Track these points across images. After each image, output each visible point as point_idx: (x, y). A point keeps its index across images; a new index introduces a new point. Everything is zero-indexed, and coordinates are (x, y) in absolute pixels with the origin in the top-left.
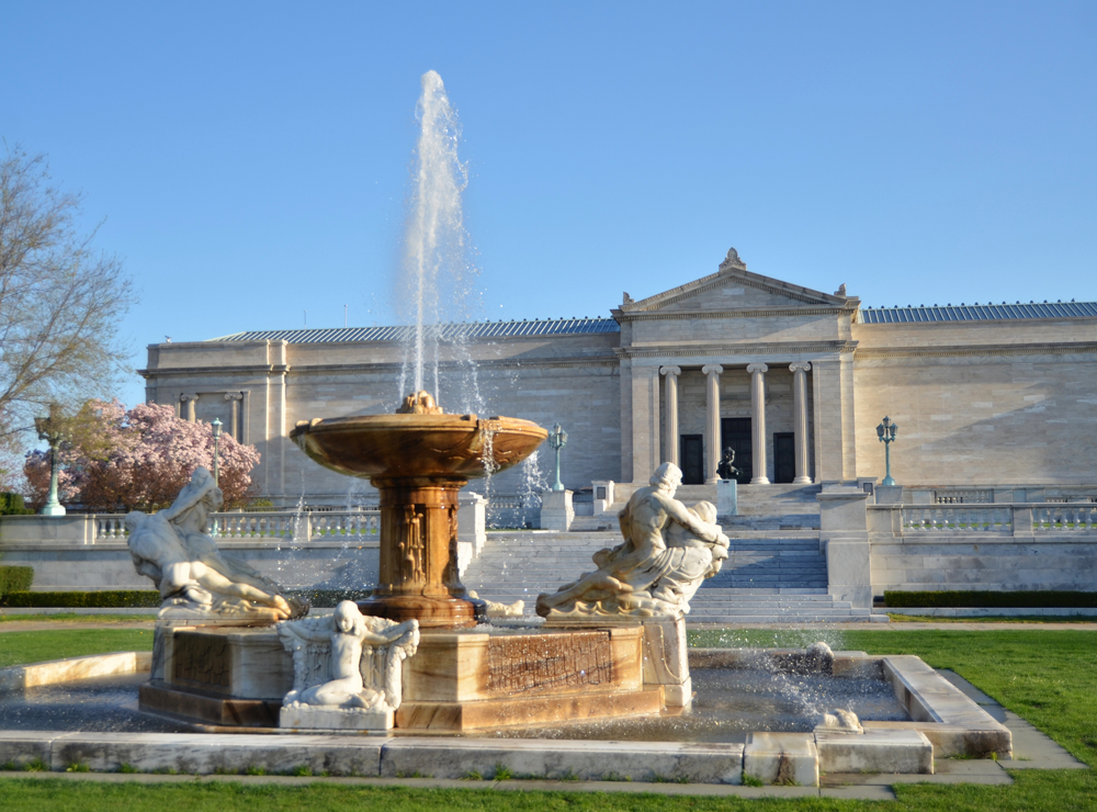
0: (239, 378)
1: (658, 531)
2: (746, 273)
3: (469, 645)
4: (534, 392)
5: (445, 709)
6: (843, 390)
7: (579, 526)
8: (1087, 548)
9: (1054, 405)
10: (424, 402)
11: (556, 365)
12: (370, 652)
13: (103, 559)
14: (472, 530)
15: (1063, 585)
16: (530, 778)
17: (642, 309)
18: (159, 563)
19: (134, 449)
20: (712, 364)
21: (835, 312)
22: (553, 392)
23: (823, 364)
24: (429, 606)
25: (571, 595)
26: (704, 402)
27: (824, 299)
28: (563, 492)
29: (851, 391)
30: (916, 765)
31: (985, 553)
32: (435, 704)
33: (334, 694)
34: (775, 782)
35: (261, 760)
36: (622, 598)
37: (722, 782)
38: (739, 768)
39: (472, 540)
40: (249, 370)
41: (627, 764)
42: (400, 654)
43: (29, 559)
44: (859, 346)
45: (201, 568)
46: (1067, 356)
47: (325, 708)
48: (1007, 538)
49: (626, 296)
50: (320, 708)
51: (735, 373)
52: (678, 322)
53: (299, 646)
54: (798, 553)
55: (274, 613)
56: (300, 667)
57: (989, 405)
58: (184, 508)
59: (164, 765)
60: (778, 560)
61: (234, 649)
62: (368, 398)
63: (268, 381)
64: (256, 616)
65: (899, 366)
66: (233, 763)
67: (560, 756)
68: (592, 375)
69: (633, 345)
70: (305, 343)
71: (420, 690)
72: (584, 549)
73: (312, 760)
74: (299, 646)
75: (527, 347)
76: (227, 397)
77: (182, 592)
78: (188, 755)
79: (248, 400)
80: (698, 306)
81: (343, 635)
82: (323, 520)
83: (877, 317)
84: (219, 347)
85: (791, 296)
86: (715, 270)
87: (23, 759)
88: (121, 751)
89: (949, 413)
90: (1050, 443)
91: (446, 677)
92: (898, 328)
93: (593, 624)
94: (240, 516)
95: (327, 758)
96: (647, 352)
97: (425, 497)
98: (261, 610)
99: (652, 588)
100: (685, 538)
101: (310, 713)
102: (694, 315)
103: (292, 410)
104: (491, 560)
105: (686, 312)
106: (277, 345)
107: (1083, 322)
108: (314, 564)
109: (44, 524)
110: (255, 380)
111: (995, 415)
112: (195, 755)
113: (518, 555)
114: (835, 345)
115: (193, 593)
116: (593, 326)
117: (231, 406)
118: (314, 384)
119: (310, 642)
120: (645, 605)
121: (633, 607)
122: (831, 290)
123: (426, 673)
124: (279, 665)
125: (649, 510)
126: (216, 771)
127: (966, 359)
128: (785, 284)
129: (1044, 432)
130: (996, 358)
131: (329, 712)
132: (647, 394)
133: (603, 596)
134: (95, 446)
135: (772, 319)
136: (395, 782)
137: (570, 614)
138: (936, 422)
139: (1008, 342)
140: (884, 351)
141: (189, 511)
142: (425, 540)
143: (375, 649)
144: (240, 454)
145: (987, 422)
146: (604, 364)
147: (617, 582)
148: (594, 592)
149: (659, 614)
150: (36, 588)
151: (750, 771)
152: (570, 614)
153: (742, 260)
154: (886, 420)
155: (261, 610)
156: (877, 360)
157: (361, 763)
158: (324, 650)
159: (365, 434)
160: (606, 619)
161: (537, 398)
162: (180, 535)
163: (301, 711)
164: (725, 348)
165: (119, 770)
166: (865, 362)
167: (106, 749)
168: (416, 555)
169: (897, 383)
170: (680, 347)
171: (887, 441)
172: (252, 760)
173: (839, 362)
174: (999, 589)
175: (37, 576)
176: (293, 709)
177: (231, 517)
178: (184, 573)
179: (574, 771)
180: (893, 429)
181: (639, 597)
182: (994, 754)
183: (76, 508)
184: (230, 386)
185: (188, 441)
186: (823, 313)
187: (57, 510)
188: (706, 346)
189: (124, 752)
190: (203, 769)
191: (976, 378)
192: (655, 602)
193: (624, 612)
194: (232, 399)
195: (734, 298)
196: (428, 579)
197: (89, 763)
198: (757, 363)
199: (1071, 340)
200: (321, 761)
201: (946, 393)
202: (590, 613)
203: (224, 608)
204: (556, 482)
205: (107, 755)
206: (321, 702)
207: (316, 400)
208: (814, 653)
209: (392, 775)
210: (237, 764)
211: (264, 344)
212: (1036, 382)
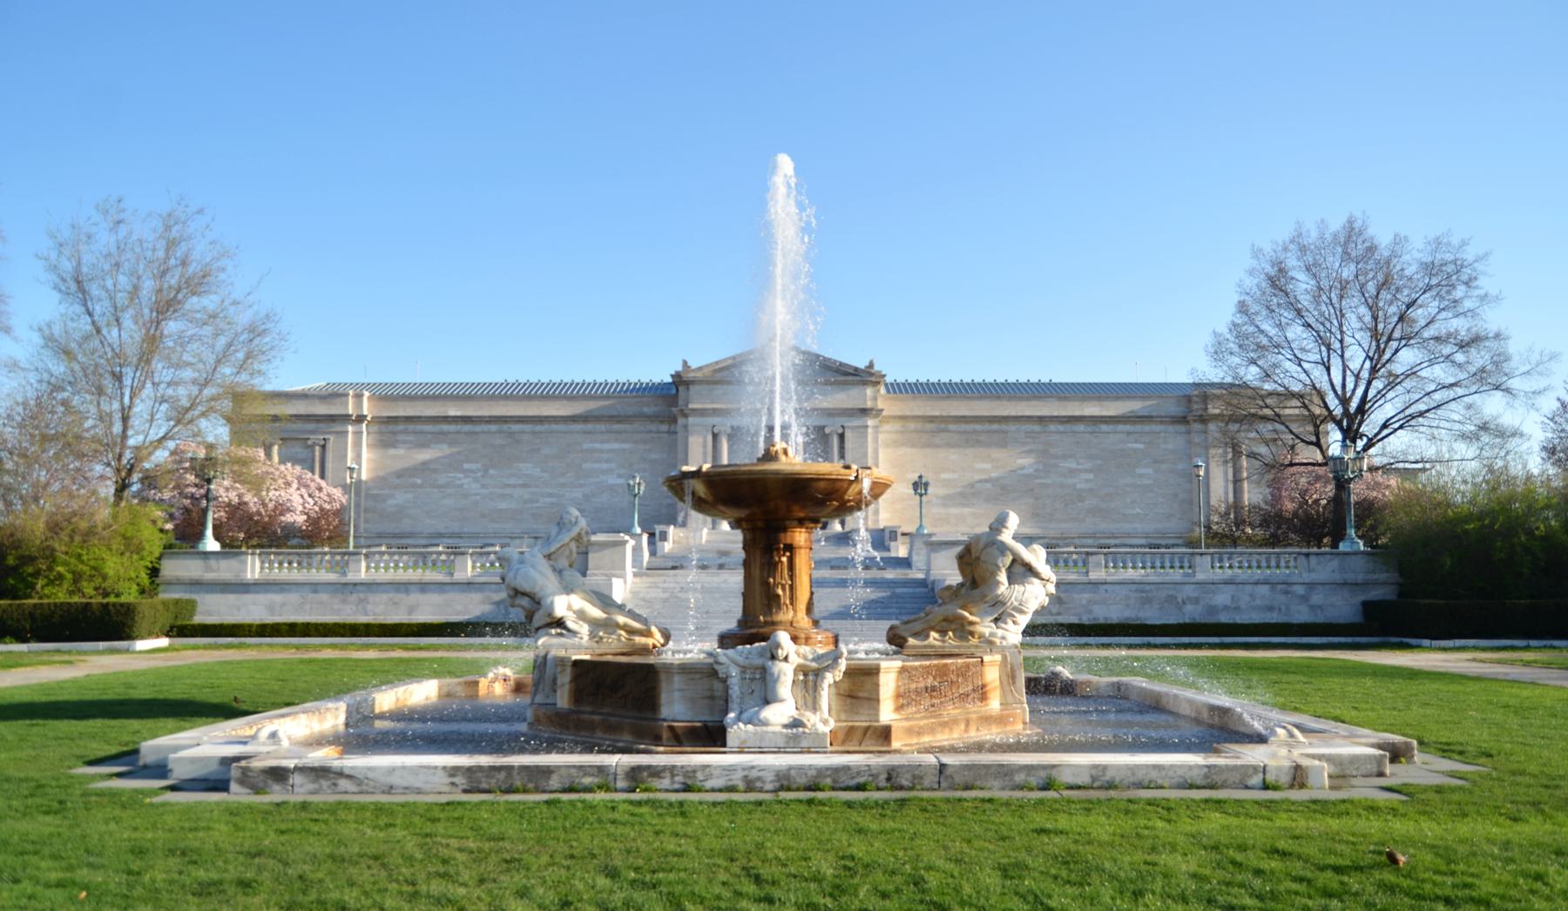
0: (322, 425)
1: (1004, 570)
3: (888, 671)
4: (598, 446)
6: (870, 450)
7: (654, 565)
8: (1148, 588)
10: (785, 452)
11: (619, 422)
12: (801, 678)
13: (266, 592)
14: (623, 568)
16: (1079, 787)
17: (699, 375)
18: (538, 596)
19: (227, 490)
21: (865, 383)
22: (616, 446)
23: (853, 428)
24: (803, 636)
25: (925, 626)
27: (856, 372)
28: (640, 535)
29: (876, 451)
30: (1375, 770)
31: (1066, 591)
32: (867, 724)
33: (778, 714)
34: (1291, 786)
35: (826, 777)
36: (971, 628)
37: (1247, 787)
38: (1261, 775)
39: (623, 576)
40: (332, 419)
41: (1164, 773)
42: (829, 678)
43: (191, 592)
44: (884, 413)
45: (577, 601)
46: (1052, 427)
47: (770, 729)
48: (1084, 579)
49: (685, 363)
50: (764, 728)
53: (734, 672)
54: (911, 590)
55: (650, 641)
56: (735, 691)
57: (987, 466)
58: (558, 545)
59: (730, 783)
60: (894, 596)
61: (663, 676)
62: (445, 446)
63: (350, 428)
64: (634, 645)
65: (916, 431)
66: (798, 780)
67: (1105, 768)
68: (651, 432)
69: (690, 406)
70: (385, 395)
71: (845, 711)
72: (723, 585)
73: (875, 776)
74: (734, 672)
75: (592, 405)
76: (310, 442)
77: (560, 623)
78: (754, 774)
79: (330, 446)
81: (777, 662)
82: (405, 558)
83: (899, 389)
84: (303, 396)
87: (587, 781)
89: (954, 472)
90: (1037, 499)
91: (869, 699)
92: (915, 398)
93: (947, 651)
94: (325, 554)
95: (889, 774)
96: (702, 413)
97: (792, 538)
98: (638, 640)
99: (996, 620)
100: (1025, 577)
101: (755, 734)
103: (372, 456)
106: (359, 396)
107: (1066, 399)
108: (476, 597)
109: (207, 558)
110: (338, 428)
111: (994, 475)
112: (761, 774)
113: (664, 590)
114: (864, 412)
115: (570, 624)
116: (657, 389)
117: (313, 452)
118: (394, 433)
119: (744, 669)
120: (992, 634)
121: (981, 636)
122: (862, 365)
124: (711, 690)
125: (996, 552)
126: (782, 788)
127: (970, 427)
129: (1032, 490)
130: (995, 427)
131: (774, 733)
132: (701, 450)
133: (953, 627)
134: (188, 485)
136: (959, 794)
137: (926, 643)
138: (945, 480)
139: (1005, 413)
140: (903, 418)
142: (792, 577)
143: (805, 675)
144: (329, 495)
145: (986, 481)
146: (662, 422)
147: (966, 614)
148: (944, 624)
149: (1004, 643)
150: (198, 619)
151: (1270, 778)
152: (926, 643)
154: (920, 477)
155: (638, 640)
156: (897, 426)
157: (921, 778)
158: (758, 676)
159: (759, 480)
160: (958, 647)
161: (601, 451)
162: (554, 570)
163: (746, 732)
165: (687, 789)
166: (887, 427)
167: (672, 769)
168: (784, 589)
169: (913, 446)
171: (921, 495)
172: (816, 777)
173: (867, 427)
174: (1077, 621)
175: (199, 608)
176: (737, 731)
177: (317, 554)
178: (563, 605)
179: (1117, 780)
180: (926, 485)
181: (985, 627)
182: (1403, 760)
183: (230, 546)
184: (313, 432)
185: (281, 481)
186: (854, 384)
187: (211, 544)
189: (691, 772)
190: (769, 787)
191: (978, 443)
192: (1000, 632)
193: (974, 641)
194: (315, 444)
196: (795, 611)
197: (656, 783)
199: (1056, 414)
200: (884, 776)
201: (953, 456)
202: (944, 641)
203: (601, 638)
204: (633, 525)
205: (673, 776)
206: (765, 723)
207: (395, 447)
209: (953, 788)
210: (802, 781)
211: (347, 395)
212: (1027, 448)
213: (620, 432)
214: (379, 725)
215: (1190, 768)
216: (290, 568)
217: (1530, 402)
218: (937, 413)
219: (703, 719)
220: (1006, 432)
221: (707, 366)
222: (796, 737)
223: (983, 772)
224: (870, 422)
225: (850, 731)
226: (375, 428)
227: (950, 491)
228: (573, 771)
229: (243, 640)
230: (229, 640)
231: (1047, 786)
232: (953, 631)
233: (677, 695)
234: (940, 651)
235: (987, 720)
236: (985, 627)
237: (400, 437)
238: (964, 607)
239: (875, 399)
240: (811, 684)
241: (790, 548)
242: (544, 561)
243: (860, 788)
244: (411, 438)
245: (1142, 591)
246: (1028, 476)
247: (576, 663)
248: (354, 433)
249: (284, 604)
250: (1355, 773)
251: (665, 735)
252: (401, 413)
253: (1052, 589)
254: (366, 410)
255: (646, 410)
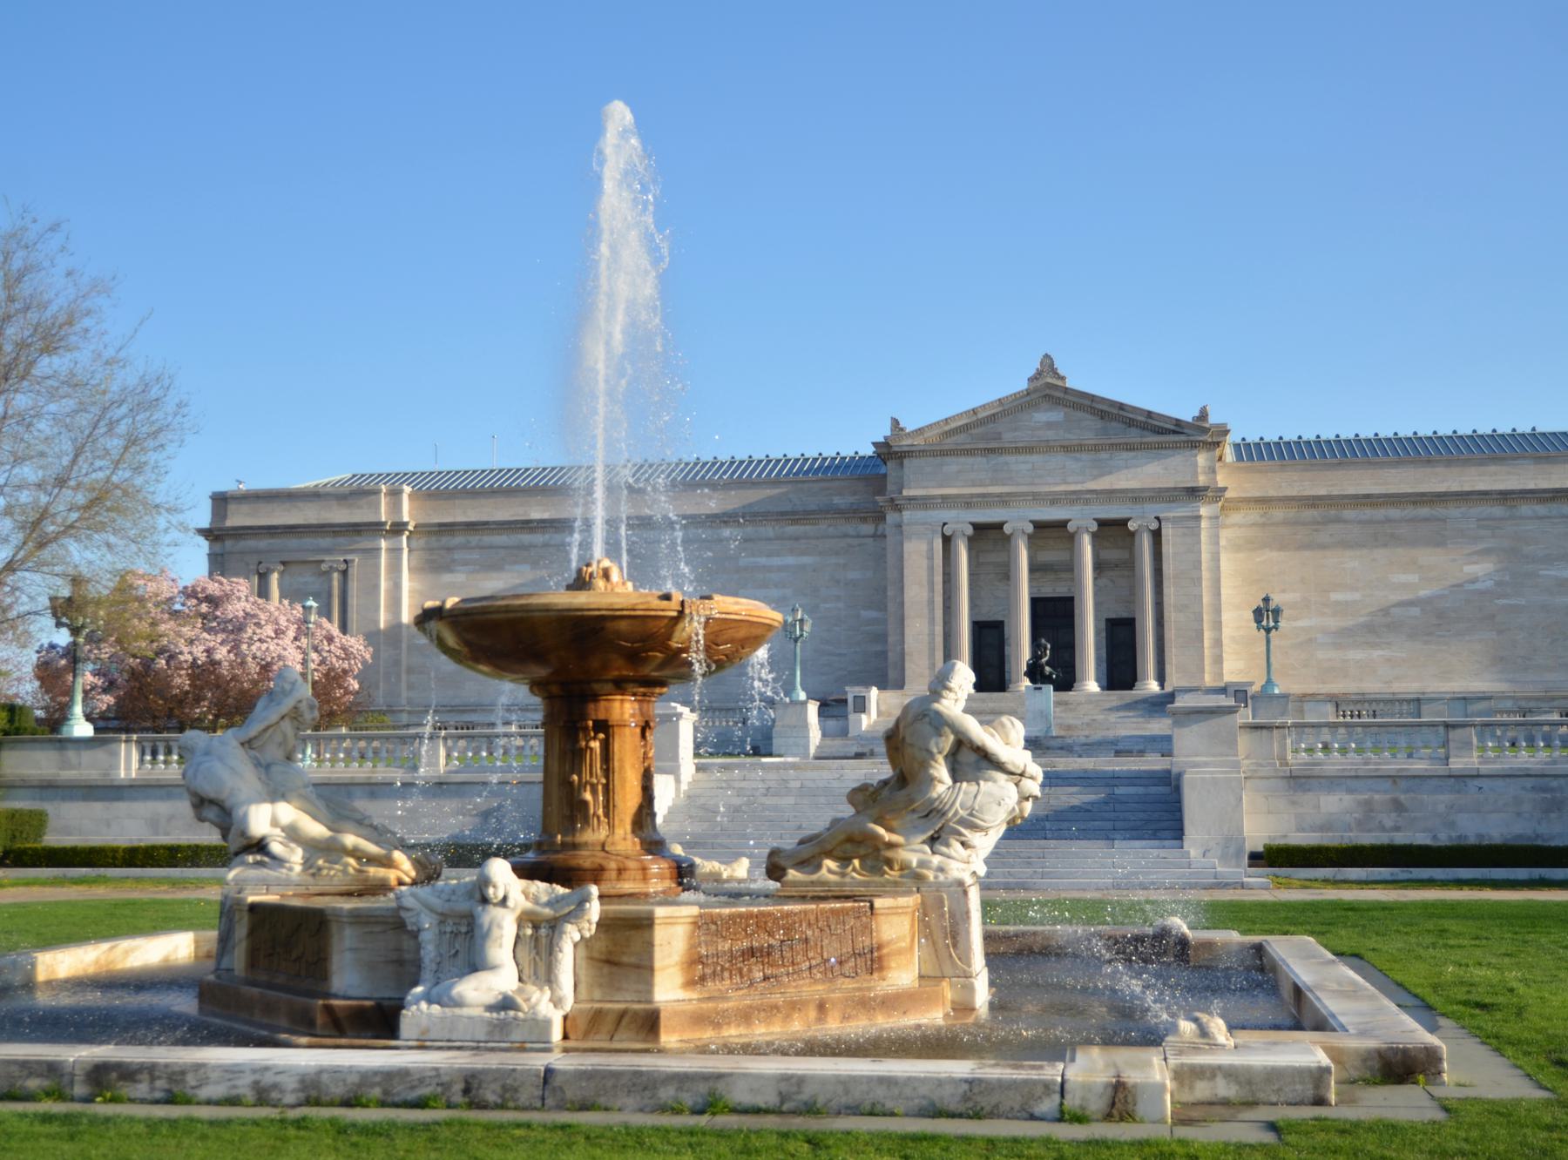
0: (341, 540)
1: (940, 759)
2: (1066, 390)
3: (671, 922)
4: (763, 561)
5: (636, 1013)
7: (827, 752)
8: (1554, 784)
9: (1507, 578)
10: (606, 574)
11: (795, 522)
12: (529, 932)
13: (147, 798)
14: (675, 757)
15: (1520, 836)
16: (758, 1111)
17: (918, 441)
18: (227, 804)
19: (191, 642)
20: (1018, 520)
21: (1194, 446)
22: (790, 560)
23: (1176, 521)
24: (613, 865)
26: (1006, 574)
27: (1178, 427)
28: (804, 703)
29: (1216, 559)
30: (1310, 1093)
32: (622, 1006)
33: (476, 991)
34: (1108, 1117)
35: (373, 1085)
36: (889, 854)
37: (1032, 1117)
38: (1057, 1097)
39: (674, 771)
40: (356, 529)
41: (896, 1091)
42: (571, 935)
43: (42, 799)
44: (1228, 494)
45: (287, 812)
46: (1525, 509)
47: (465, 1011)
48: (1440, 769)
49: (895, 422)
50: (457, 1011)
51: (1050, 532)
52: (970, 460)
53: (427, 923)
54: (1141, 790)
55: (391, 875)
56: (429, 952)
57: (1413, 578)
58: (260, 727)
59: (234, 1092)
60: (1111, 800)
61: (334, 928)
62: (526, 568)
63: (383, 544)
64: (366, 880)
65: (1286, 523)
67: (800, 1081)
68: (846, 536)
69: (905, 493)
70: (434, 490)
71: (601, 985)
73: (446, 1086)
74: (427, 923)
76: (324, 567)
77: (260, 846)
78: (268, 1079)
79: (354, 571)
80: (998, 437)
81: (491, 908)
83: (1255, 453)
84: (313, 495)
85: (1131, 423)
86: (1023, 385)
87: (33, 1084)
88: (174, 1073)
91: (638, 967)
93: (847, 890)
94: (342, 738)
95: (467, 1082)
96: (925, 503)
97: (607, 710)
98: (374, 872)
99: (933, 841)
100: (979, 769)
101: (443, 1019)
102: (992, 451)
103: (417, 585)
104: (702, 801)
105: (981, 446)
106: (395, 494)
107: (1548, 460)
109: (62, 748)
110: (365, 543)
111: (1422, 593)
112: (279, 1079)
113: (740, 792)
115: (276, 848)
117: (330, 580)
118: (449, 549)
119: (443, 917)
120: (922, 864)
121: (904, 867)
122: (1187, 414)
123: (609, 962)
124: (399, 950)
125: (928, 729)
126: (309, 1102)
127: (1380, 513)
128: (1121, 406)
130: (1424, 511)
131: (470, 1018)
132: (925, 563)
133: (862, 851)
134: (136, 638)
135: (1104, 455)
137: (814, 877)
138: (1338, 603)
140: (1263, 501)
141: (270, 731)
142: (607, 772)
143: (536, 927)
144: (344, 649)
145: (1411, 603)
146: (864, 520)
147: (881, 831)
148: (848, 846)
149: (942, 877)
150: (52, 839)
151: (1072, 1102)
152: (814, 877)
153: (1061, 372)
154: (1266, 600)
155: (374, 872)
156: (1254, 515)
157: (516, 1090)
158: (464, 929)
161: (769, 569)
162: (257, 764)
163: (430, 1016)
164: (1036, 498)
165: (171, 1099)
166: (1236, 517)
167: (151, 1070)
168: (594, 792)
169: (1282, 547)
170: (972, 496)
171: (1268, 630)
172: (360, 1085)
173: (1199, 518)
175: (52, 823)
176: (419, 1013)
177: (331, 738)
178: (262, 819)
180: (1277, 612)
181: (913, 852)
182: (1421, 1078)
183: (109, 725)
184: (328, 551)
186: (1176, 447)
188: (1008, 494)
189: (176, 1075)
190: (290, 1099)
191: (1394, 540)
195: (1050, 425)
196: (611, 826)
198: (1082, 519)
199: (1531, 486)
201: (1351, 562)
202: (843, 875)
203: (320, 869)
204: (794, 688)
205: (153, 1079)
206: (458, 1003)
208: (1163, 934)
209: (561, 1107)
210: (338, 1091)
211: (377, 492)
213: (797, 539)
214: (43, 999)
215: (940, 1083)
216: (334, 761)
217: (630, 465)
218: (1323, 492)
219: (377, 995)
220: (1444, 520)
221: (931, 426)
222: (502, 1026)
223: (610, 1084)
224: (1204, 511)
225: (596, 1018)
226: (420, 542)
227: (1349, 622)
228: (14, 1070)
229: (102, 871)
230: (84, 870)
231: (710, 1105)
232: (862, 859)
233: (348, 956)
234: (836, 891)
235: (891, 1002)
236: (913, 852)
237: (457, 555)
238: (879, 821)
239: (1213, 471)
240: (544, 941)
241: (604, 727)
242: (240, 752)
243: (421, 1104)
244: (475, 556)
245: (1544, 790)
246: (1482, 593)
247: (254, 908)
248: (389, 550)
249: (171, 818)
250: (1274, 1099)
251: (320, 1019)
252: (461, 518)
253: (1033, 787)
254: (407, 513)
255: (837, 500)
